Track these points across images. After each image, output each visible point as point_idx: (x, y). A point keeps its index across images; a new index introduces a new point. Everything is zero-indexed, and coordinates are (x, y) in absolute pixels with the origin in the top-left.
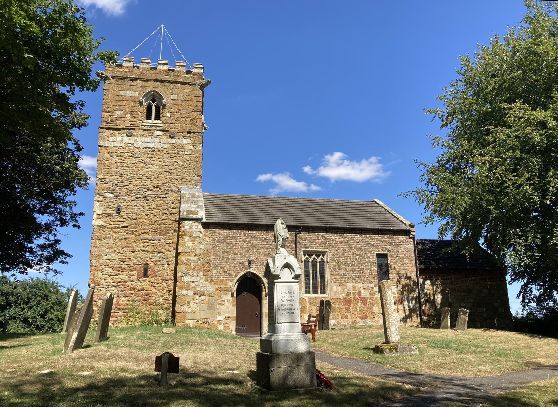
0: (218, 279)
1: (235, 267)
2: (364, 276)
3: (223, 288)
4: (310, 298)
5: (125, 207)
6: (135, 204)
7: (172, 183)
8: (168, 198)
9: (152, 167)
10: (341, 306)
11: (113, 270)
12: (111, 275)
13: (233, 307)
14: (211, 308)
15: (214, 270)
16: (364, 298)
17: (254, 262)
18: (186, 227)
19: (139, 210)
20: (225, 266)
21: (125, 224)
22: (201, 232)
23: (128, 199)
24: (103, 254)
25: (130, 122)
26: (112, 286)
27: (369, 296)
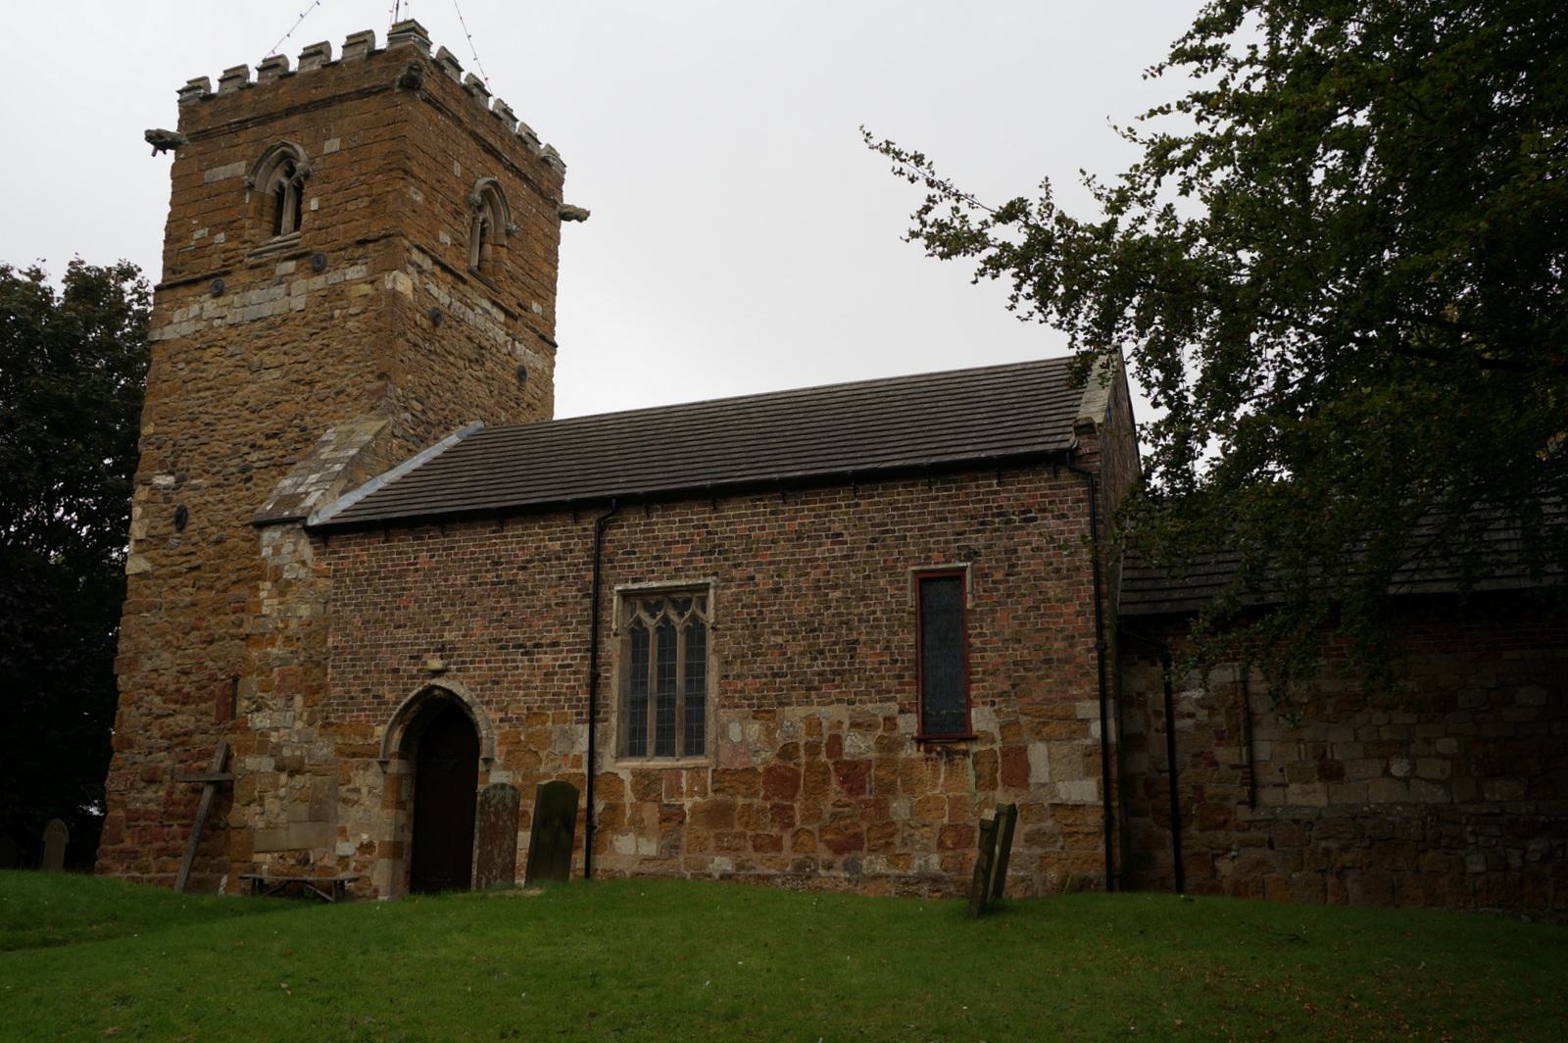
0: (344, 717)
1: (396, 671)
4: (640, 775)
7: (311, 416)
9: (267, 376)
10: (757, 802)
12: (159, 717)
13: (384, 813)
15: (336, 685)
16: (854, 765)
17: (455, 649)
20: (367, 672)
21: (195, 561)
22: (304, 563)
25: (224, 252)
26: (160, 750)
27: (872, 755)
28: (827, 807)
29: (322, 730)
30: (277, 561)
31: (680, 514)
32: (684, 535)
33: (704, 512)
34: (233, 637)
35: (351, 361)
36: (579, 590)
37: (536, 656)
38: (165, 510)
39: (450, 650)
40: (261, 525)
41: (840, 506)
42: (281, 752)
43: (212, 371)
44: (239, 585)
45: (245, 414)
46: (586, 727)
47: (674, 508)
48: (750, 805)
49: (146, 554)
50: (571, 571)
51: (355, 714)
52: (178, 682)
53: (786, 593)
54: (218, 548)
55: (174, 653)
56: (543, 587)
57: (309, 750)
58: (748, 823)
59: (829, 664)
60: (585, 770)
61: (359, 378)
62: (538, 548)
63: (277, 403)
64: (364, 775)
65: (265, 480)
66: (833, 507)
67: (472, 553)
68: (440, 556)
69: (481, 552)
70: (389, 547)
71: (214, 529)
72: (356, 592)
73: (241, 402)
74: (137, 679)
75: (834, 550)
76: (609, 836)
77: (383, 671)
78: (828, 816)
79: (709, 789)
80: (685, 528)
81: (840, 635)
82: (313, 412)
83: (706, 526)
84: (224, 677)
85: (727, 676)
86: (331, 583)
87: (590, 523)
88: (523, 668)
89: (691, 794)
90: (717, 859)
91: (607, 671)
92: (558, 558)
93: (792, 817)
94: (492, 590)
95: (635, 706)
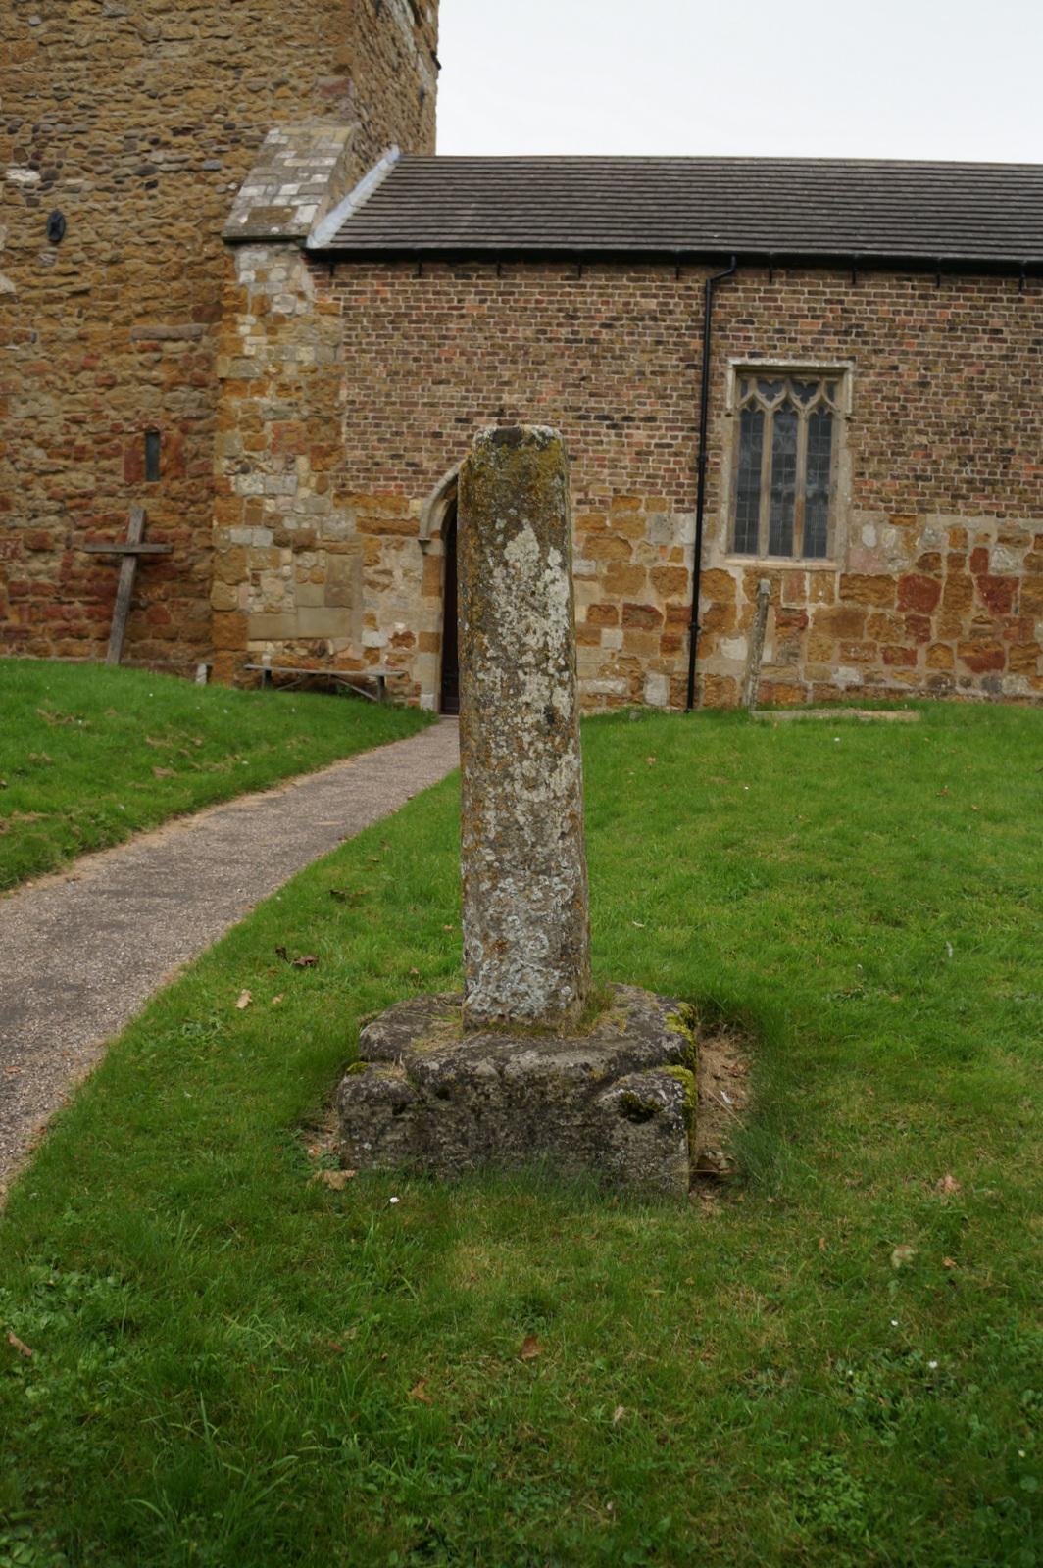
0: (366, 486)
1: (437, 435)
2: (1012, 483)
3: (385, 522)
4: (755, 575)
5: (77, 218)
6: (114, 203)
7: (240, 111)
8: (225, 171)
9: (168, 50)
10: (890, 613)
11: (49, 456)
13: (425, 600)
14: (338, 598)
15: (354, 448)
16: (1000, 581)
17: (518, 415)
18: (243, 277)
19: (123, 226)
20: (397, 434)
21: (80, 284)
22: (301, 295)
23: (88, 186)
24: (13, 399)
26: (48, 513)
27: (1021, 573)
28: (967, 623)
29: (337, 501)
30: (262, 289)
31: (810, 284)
32: (814, 309)
33: (840, 286)
34: (142, 381)
35: (295, 44)
36: (681, 359)
37: (627, 431)
38: (30, 215)
39: (511, 415)
40: (237, 242)
41: (1000, 300)
42: (281, 523)
43: (83, 34)
44: (148, 318)
45: (141, 98)
46: (693, 515)
47: (802, 277)
48: (883, 615)
49: (7, 270)
50: (671, 336)
51: (382, 483)
52: (68, 433)
53: (934, 389)
54: (112, 269)
55: (59, 398)
56: (634, 350)
57: (322, 523)
58: (878, 634)
59: (980, 473)
60: (688, 564)
61: (307, 69)
62: (627, 304)
63: (189, 88)
64: (397, 556)
65: (177, 188)
66: (993, 300)
67: (538, 301)
68: (494, 301)
69: (551, 302)
70: (421, 284)
71: (106, 245)
72: (378, 336)
73: (133, 82)
74: (9, 426)
75: (991, 348)
76: (716, 639)
77: (419, 434)
78: (967, 633)
79: (837, 596)
80: (816, 301)
81: (994, 442)
82: (242, 105)
83: (841, 302)
84: (133, 429)
85: (862, 474)
86: (341, 322)
87: (696, 281)
88: (609, 443)
89: (815, 599)
90: (843, 670)
91: (716, 455)
92: (654, 319)
93: (927, 631)
94: (567, 348)
95: (746, 498)
